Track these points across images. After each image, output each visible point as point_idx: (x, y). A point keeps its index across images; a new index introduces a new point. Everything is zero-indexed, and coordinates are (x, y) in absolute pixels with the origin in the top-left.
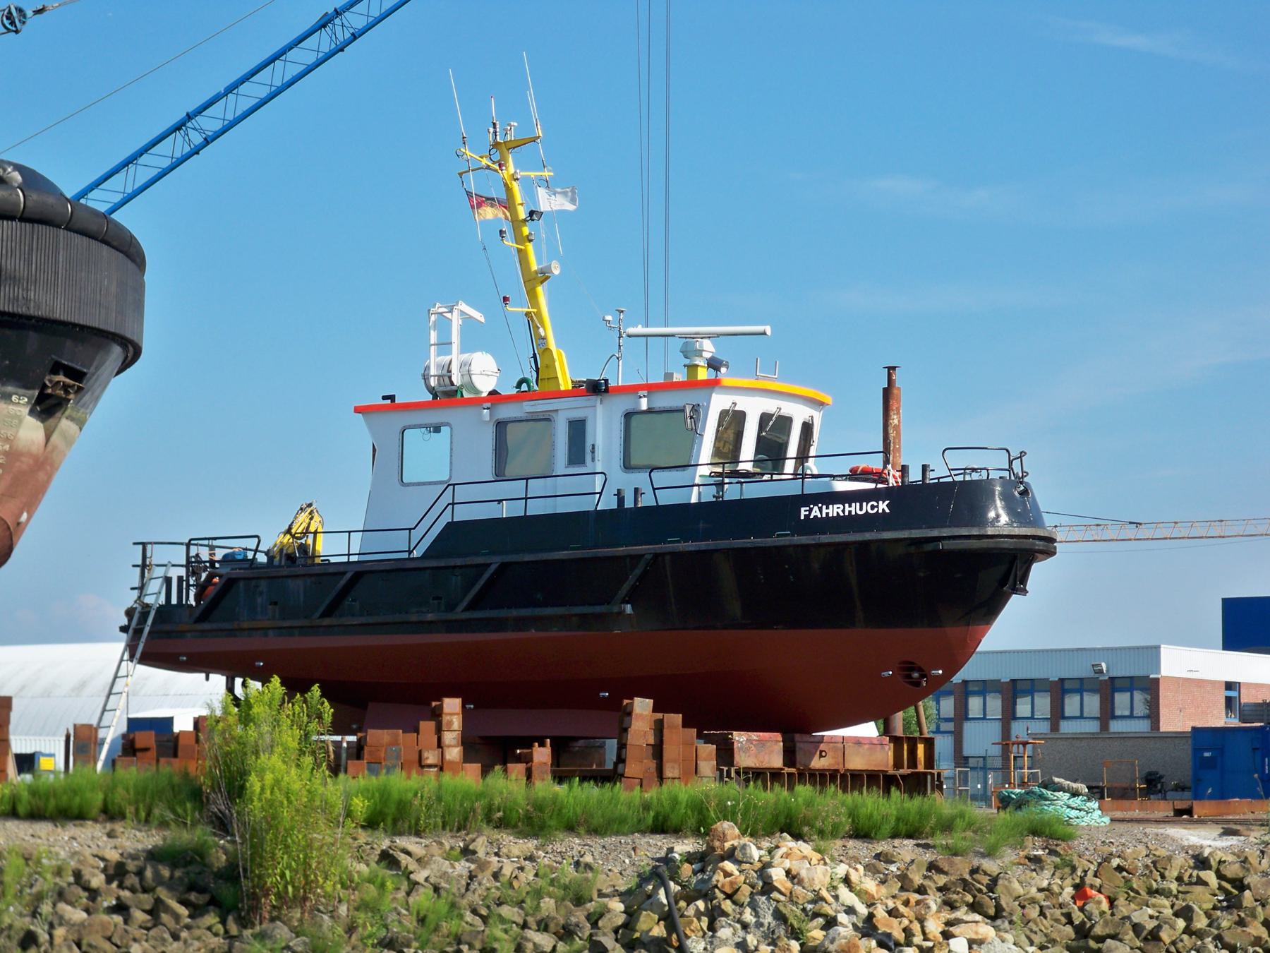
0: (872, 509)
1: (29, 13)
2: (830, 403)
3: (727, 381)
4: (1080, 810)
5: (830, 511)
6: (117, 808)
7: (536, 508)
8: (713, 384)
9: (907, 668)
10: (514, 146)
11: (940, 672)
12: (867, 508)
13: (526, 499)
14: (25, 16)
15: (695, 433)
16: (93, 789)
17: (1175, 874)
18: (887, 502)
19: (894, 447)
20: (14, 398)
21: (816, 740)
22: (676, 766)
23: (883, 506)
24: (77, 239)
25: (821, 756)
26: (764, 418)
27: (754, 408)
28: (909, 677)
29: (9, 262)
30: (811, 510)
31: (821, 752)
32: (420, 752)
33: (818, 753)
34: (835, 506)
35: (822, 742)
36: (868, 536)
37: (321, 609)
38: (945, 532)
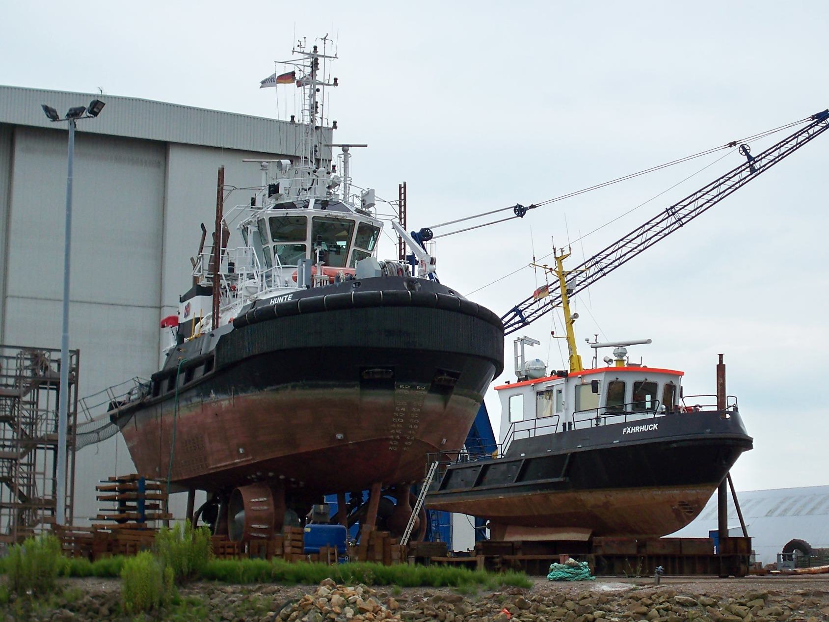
0: (651, 428)
5: (634, 430)
6: (66, 554)
7: (540, 433)
18: (657, 424)
23: (655, 426)
30: (627, 430)
34: (637, 427)
37: (515, 480)
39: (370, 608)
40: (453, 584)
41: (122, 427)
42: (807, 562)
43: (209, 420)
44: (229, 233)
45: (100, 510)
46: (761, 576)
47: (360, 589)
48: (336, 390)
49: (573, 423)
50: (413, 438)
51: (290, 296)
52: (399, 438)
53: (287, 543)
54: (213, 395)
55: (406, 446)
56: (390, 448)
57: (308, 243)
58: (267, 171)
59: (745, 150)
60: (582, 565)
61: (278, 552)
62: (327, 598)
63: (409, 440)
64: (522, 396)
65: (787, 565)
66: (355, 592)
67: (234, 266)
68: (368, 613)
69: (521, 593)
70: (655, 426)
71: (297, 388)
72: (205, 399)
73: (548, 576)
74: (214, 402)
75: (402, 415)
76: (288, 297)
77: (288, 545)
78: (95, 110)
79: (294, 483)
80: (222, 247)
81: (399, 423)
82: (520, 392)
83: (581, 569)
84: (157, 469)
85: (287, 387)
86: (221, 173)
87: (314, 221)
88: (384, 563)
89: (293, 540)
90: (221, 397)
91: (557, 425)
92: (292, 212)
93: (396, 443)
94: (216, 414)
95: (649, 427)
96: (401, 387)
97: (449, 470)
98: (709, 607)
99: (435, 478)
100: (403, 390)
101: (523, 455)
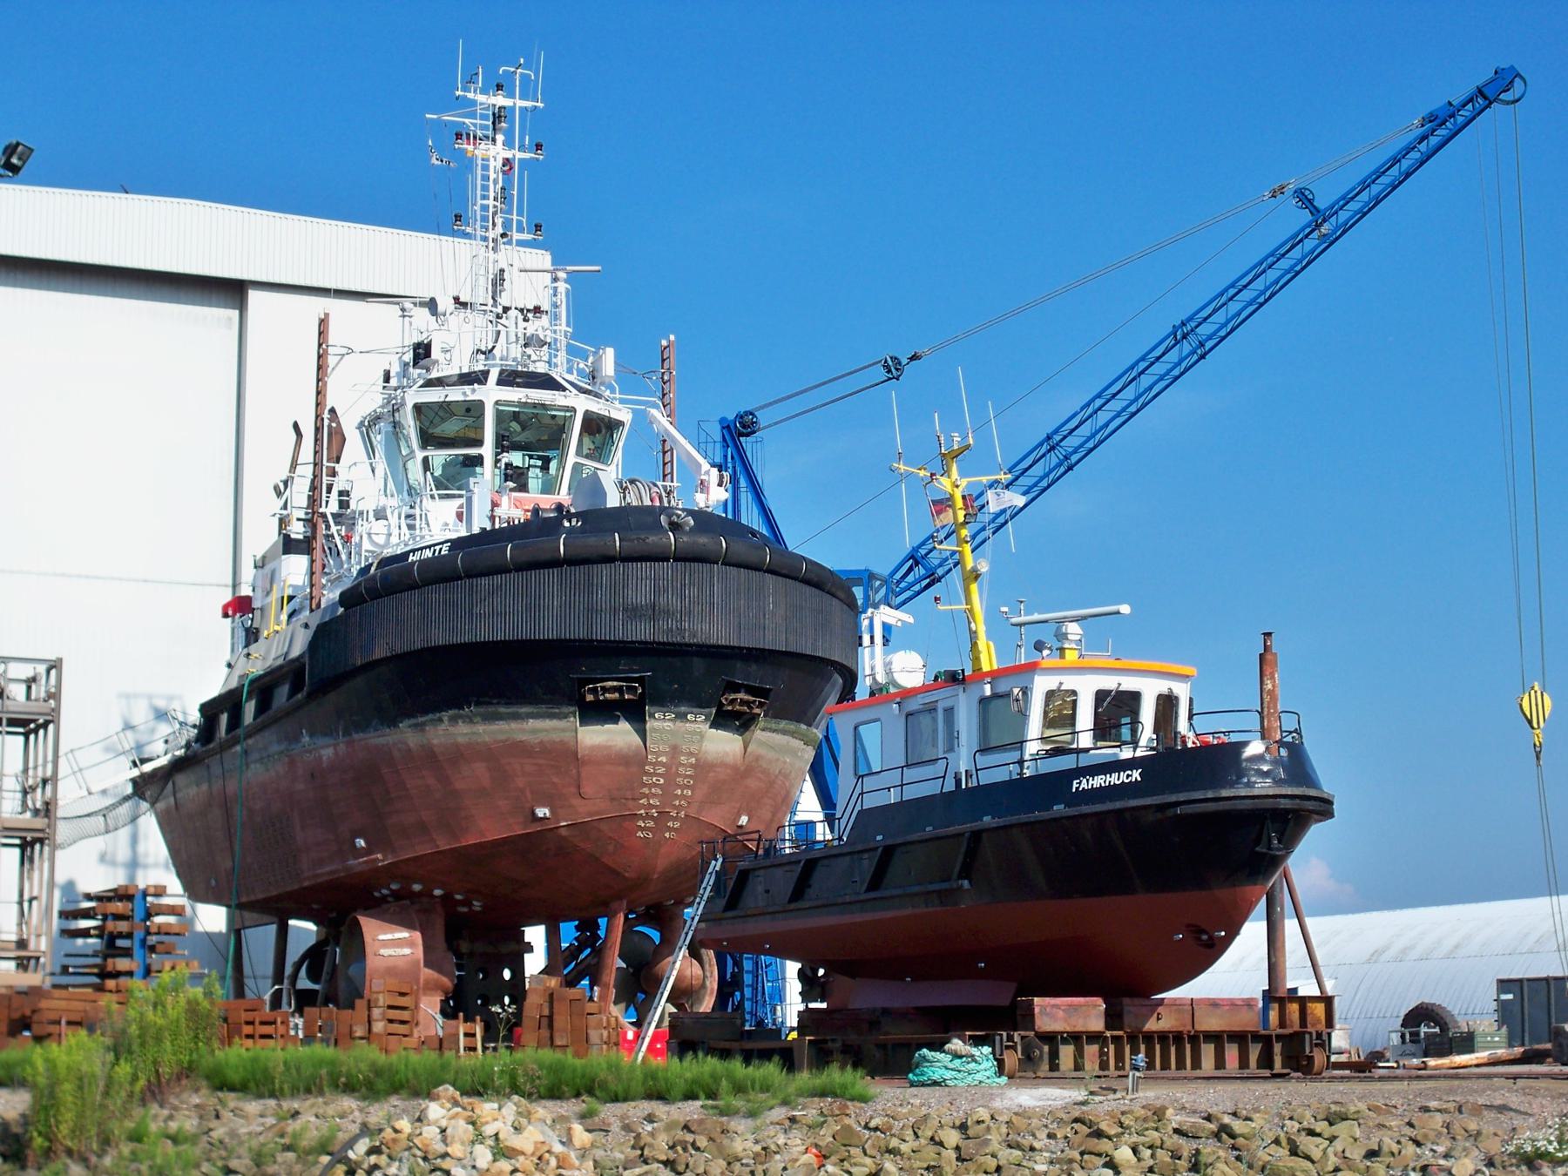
1: (904, 361)
2: (1195, 674)
3: (1045, 664)
4: (959, 1071)
5: (1095, 782)
7: (911, 793)
8: (1032, 668)
9: (1196, 930)
10: (955, 455)
11: (1223, 933)
12: (1123, 777)
13: (902, 785)
14: (900, 363)
15: (1023, 715)
16: (362, 1061)
17: (930, 1134)
18: (1140, 770)
19: (1269, 711)
20: (689, 716)
21: (1154, 1002)
22: (564, 1034)
23: (1136, 775)
24: (733, 571)
25: (1158, 1019)
26: (1101, 696)
27: (1086, 688)
28: (1200, 939)
29: (661, 599)
30: (1080, 783)
31: (1159, 1014)
32: (351, 1026)
33: (1155, 1015)
35: (1161, 1005)
36: (1118, 805)
38: (1182, 797)
39: (529, 1148)
40: (712, 1095)
41: (153, 804)
42: (1446, 1046)
43: (300, 786)
44: (344, 440)
45: (67, 955)
46: (1360, 1072)
47: (510, 1109)
48: (532, 723)
49: (974, 772)
50: (682, 814)
51: (445, 548)
52: (656, 815)
53: (376, 1012)
54: (306, 739)
55: (670, 829)
56: (639, 834)
57: (487, 450)
58: (412, 319)
59: (1304, 198)
60: (978, 1053)
61: (359, 1031)
62: (439, 1127)
63: (675, 819)
64: (879, 723)
65: (1408, 1052)
66: (498, 1115)
67: (348, 496)
68: (521, 1158)
69: (848, 1112)
70: (1136, 775)
71: (460, 722)
72: (293, 747)
73: (911, 1076)
74: (306, 752)
75: (661, 770)
76: (441, 549)
77: (380, 1017)
78: (14, 160)
79: (462, 903)
80: (328, 461)
81: (655, 785)
82: (872, 717)
83: (976, 1062)
84: (213, 882)
85: (441, 720)
86: (323, 323)
87: (497, 410)
88: (577, 1055)
89: (390, 1007)
90: (321, 741)
91: (944, 777)
92: (456, 394)
93: (651, 824)
94: (312, 775)
95: (1123, 776)
96: (656, 715)
97: (741, 871)
98: (1241, 1139)
99: (717, 888)
100: (660, 723)
101: (879, 838)
